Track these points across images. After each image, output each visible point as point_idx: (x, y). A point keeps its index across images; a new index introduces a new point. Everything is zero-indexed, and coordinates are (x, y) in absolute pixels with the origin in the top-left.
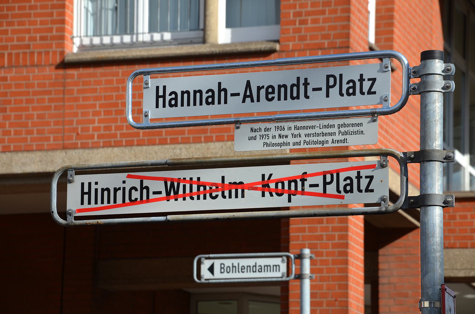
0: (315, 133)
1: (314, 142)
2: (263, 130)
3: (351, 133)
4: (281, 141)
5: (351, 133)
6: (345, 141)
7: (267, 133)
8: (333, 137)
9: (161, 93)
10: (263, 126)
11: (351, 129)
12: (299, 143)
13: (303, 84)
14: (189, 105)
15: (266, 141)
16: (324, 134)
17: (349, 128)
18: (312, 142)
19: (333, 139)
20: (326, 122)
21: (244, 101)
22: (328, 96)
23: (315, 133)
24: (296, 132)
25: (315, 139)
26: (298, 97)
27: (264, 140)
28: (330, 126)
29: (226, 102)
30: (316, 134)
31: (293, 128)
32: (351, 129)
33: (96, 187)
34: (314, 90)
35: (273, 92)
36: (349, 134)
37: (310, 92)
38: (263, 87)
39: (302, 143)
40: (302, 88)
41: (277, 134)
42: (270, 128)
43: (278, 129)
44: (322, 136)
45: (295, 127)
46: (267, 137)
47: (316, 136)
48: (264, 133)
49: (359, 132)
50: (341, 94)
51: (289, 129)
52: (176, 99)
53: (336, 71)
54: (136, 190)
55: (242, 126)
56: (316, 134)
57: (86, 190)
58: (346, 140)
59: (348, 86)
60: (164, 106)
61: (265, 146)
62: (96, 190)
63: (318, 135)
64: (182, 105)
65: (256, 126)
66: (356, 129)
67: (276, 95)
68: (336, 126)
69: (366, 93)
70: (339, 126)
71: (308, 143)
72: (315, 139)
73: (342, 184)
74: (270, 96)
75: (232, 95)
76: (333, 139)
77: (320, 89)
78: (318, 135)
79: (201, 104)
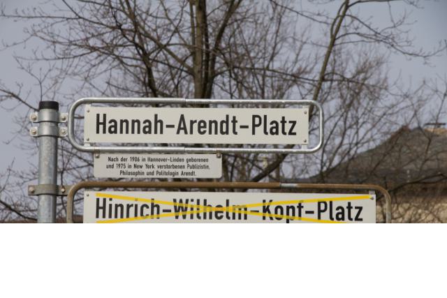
4: (136, 170)
6: (192, 173)
7: (123, 162)
10: (120, 156)
11: (198, 163)
12: (153, 173)
14: (127, 132)
15: (123, 169)
21: (178, 133)
22: (254, 133)
25: (167, 170)
26: (227, 133)
29: (161, 132)
32: (198, 163)
33: (111, 202)
34: (242, 127)
37: (238, 129)
38: (196, 121)
39: (155, 173)
40: (231, 125)
41: (132, 163)
52: (115, 126)
53: (261, 112)
54: (148, 207)
57: (101, 204)
60: (104, 132)
62: (111, 205)
64: (156, 132)
65: (113, 156)
66: (202, 163)
67: (207, 129)
68: (185, 160)
71: (160, 174)
72: (167, 170)
73: (335, 212)
74: (202, 130)
75: (168, 126)
77: (247, 127)
78: (168, 167)
79: (139, 132)
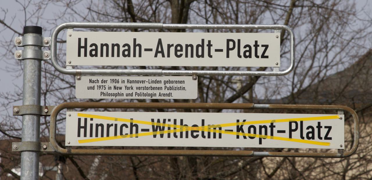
0: (145, 87)
1: (144, 94)
2: (100, 82)
3: (175, 88)
4: (116, 91)
5: (175, 88)
6: (170, 95)
7: (104, 84)
8: (160, 91)
9: (83, 44)
10: (100, 78)
11: (175, 85)
12: (131, 95)
13: (207, 45)
15: (103, 91)
16: (153, 88)
17: (173, 85)
18: (143, 94)
19: (160, 93)
20: (154, 78)
21: (156, 56)
22: (228, 56)
23: (145, 87)
24: (129, 85)
25: (145, 92)
27: (101, 91)
28: (104, 82)
29: (140, 56)
30: (146, 88)
31: (126, 81)
32: (175, 85)
33: (92, 122)
34: (217, 50)
35: (181, 50)
36: (173, 89)
39: (134, 94)
41: (112, 85)
42: (107, 81)
43: (113, 81)
44: (151, 90)
45: (128, 81)
46: (103, 88)
47: (146, 89)
48: (101, 84)
49: (181, 88)
50: (240, 56)
51: (123, 82)
53: (235, 36)
54: (127, 126)
55: (83, 78)
56: (146, 88)
57: (82, 124)
58: (171, 94)
59: (124, 48)
61: (102, 95)
62: (91, 125)
63: (147, 88)
65: (94, 78)
66: (179, 85)
68: (163, 82)
69: (260, 57)
70: (165, 82)
72: (145, 92)
75: (146, 50)
76: (160, 93)
77: (221, 50)
78: (147, 88)
